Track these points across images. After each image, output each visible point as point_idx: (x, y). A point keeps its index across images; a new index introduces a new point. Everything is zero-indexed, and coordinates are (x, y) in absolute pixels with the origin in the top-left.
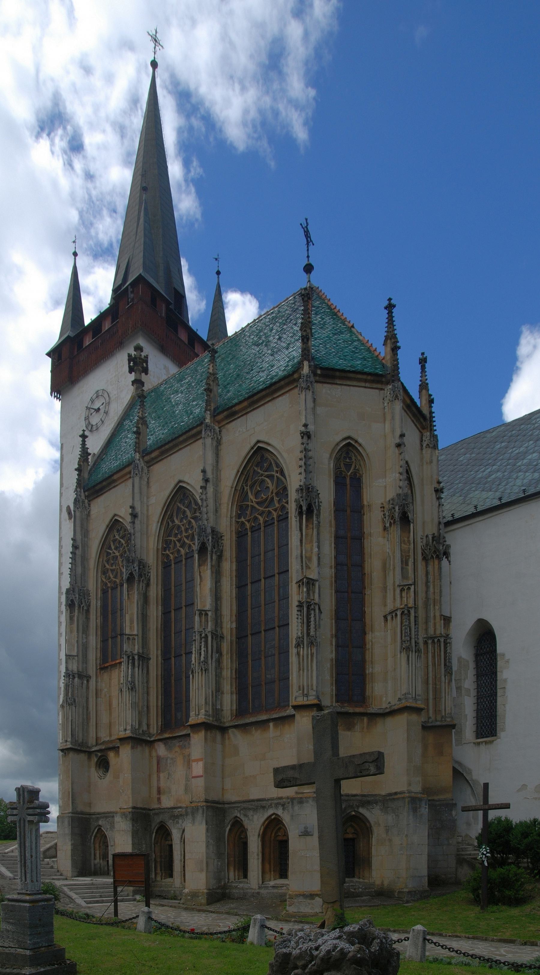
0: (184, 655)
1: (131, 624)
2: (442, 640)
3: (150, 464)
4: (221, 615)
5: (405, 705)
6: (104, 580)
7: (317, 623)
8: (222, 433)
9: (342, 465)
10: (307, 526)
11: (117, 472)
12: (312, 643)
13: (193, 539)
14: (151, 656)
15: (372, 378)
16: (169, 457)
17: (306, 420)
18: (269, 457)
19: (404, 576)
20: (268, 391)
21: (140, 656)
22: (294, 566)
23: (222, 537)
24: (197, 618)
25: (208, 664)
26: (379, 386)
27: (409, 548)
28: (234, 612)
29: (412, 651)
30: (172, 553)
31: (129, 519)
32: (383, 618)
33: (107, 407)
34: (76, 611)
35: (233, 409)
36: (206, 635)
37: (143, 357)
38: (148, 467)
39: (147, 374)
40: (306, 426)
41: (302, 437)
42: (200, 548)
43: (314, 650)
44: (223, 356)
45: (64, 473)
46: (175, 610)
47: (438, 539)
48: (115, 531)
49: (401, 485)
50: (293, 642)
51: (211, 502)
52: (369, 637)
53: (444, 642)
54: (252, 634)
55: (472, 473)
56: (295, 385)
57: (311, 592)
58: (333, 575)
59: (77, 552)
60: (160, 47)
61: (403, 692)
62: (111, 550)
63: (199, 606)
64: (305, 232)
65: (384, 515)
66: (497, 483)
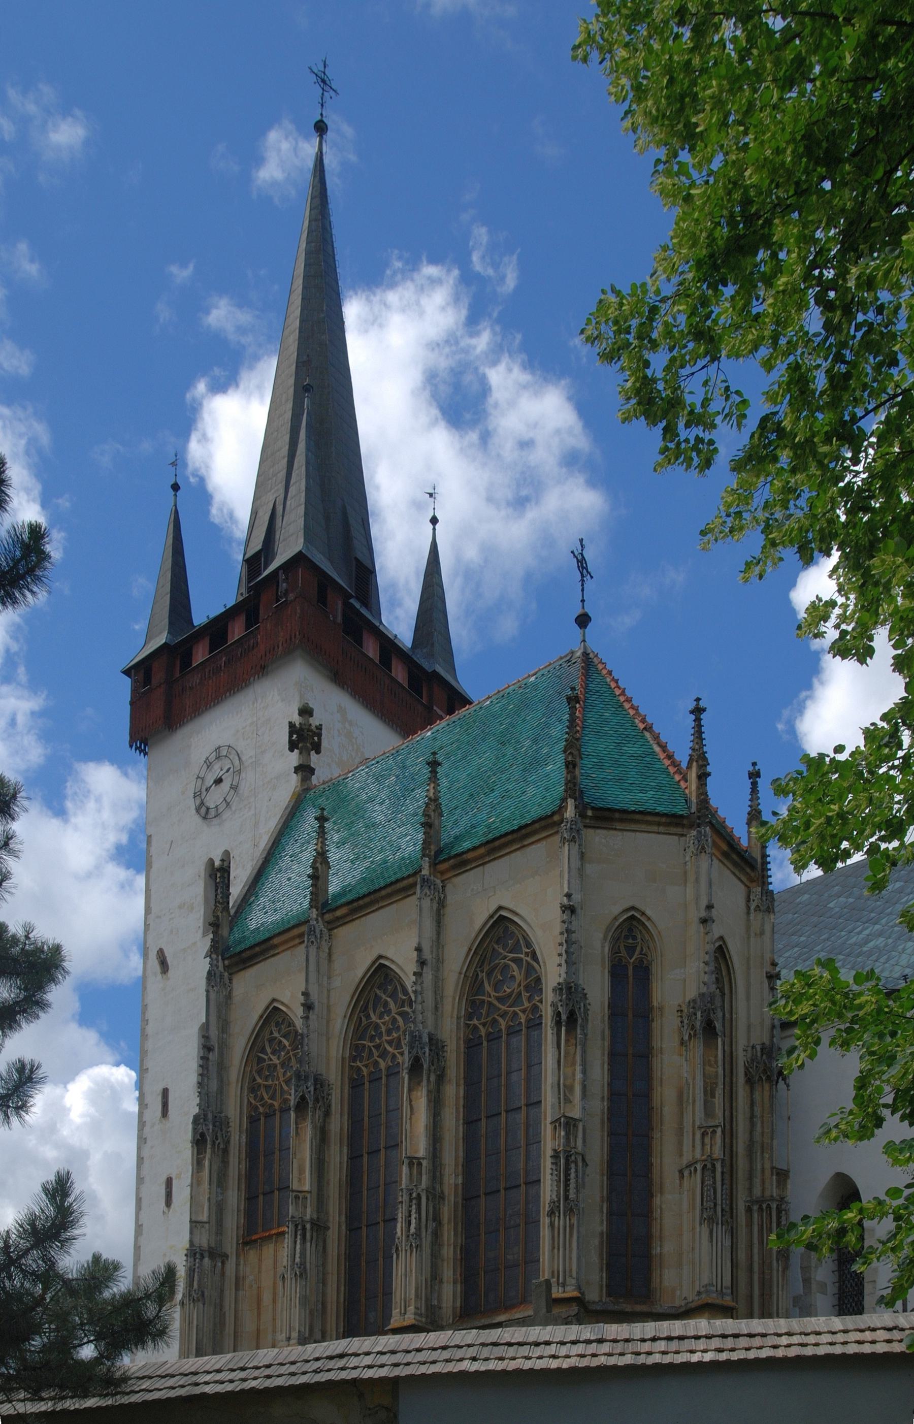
0: (382, 1224)
1: (300, 1174)
2: (774, 1206)
3: (333, 925)
4: (441, 1165)
5: (705, 1302)
6: (253, 1102)
7: (580, 1180)
8: (447, 889)
9: (622, 949)
10: (567, 1041)
11: (280, 934)
12: (571, 1210)
13: (398, 1046)
14: (331, 1225)
15: (668, 820)
16: (364, 918)
17: (569, 888)
18: (516, 932)
19: (709, 1111)
20: (515, 836)
21: (313, 1223)
22: (549, 1097)
23: (443, 1047)
24: (405, 1169)
25: (421, 1239)
26: (679, 830)
27: (717, 1072)
28: (461, 1160)
29: (717, 1224)
30: (366, 1066)
31: (300, 1011)
32: (677, 1173)
33: (236, 778)
34: (209, 1151)
35: (465, 856)
36: (419, 1195)
37: (313, 728)
38: (330, 930)
39: (318, 752)
40: (568, 896)
41: (564, 912)
42: (412, 1065)
43: (574, 1221)
44: (448, 749)
45: (153, 888)
46: (368, 1153)
47: (769, 1051)
48: (273, 1024)
49: (706, 980)
50: (545, 1207)
51: (429, 996)
52: (657, 1200)
53: (777, 1208)
54: (486, 1194)
55: (843, 933)
56: (555, 829)
57: (571, 1137)
58: (606, 1110)
59: (211, 1056)
60: (332, 93)
61: (703, 1283)
62: (267, 1054)
63: (406, 1150)
64: (578, 561)
65: (682, 1022)
66: (874, 957)
